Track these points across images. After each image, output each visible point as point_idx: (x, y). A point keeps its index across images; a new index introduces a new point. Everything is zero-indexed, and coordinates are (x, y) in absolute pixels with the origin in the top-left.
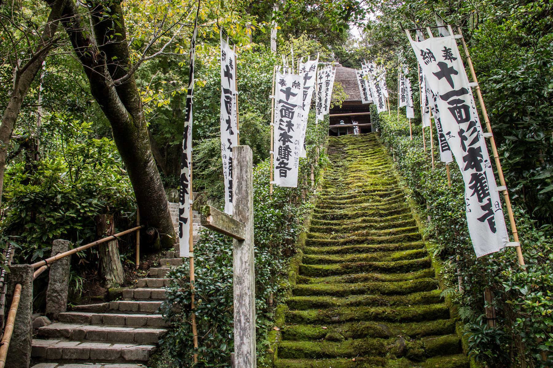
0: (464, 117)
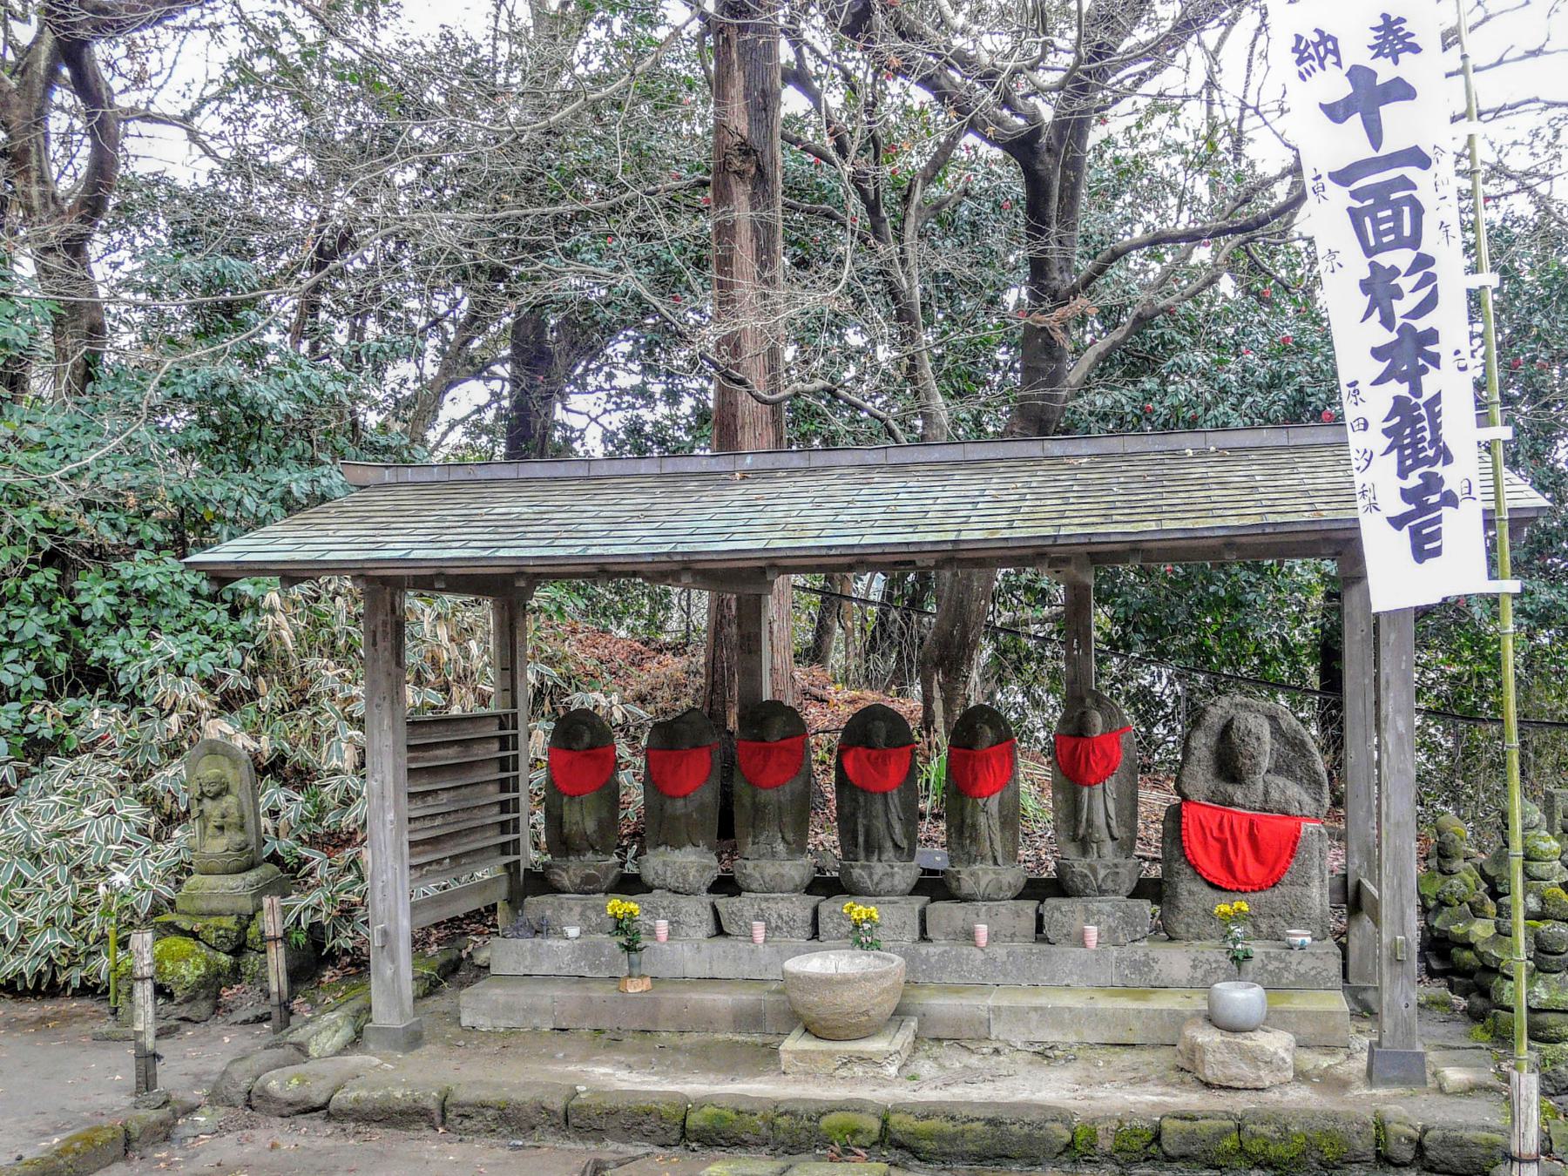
0: (1407, 232)
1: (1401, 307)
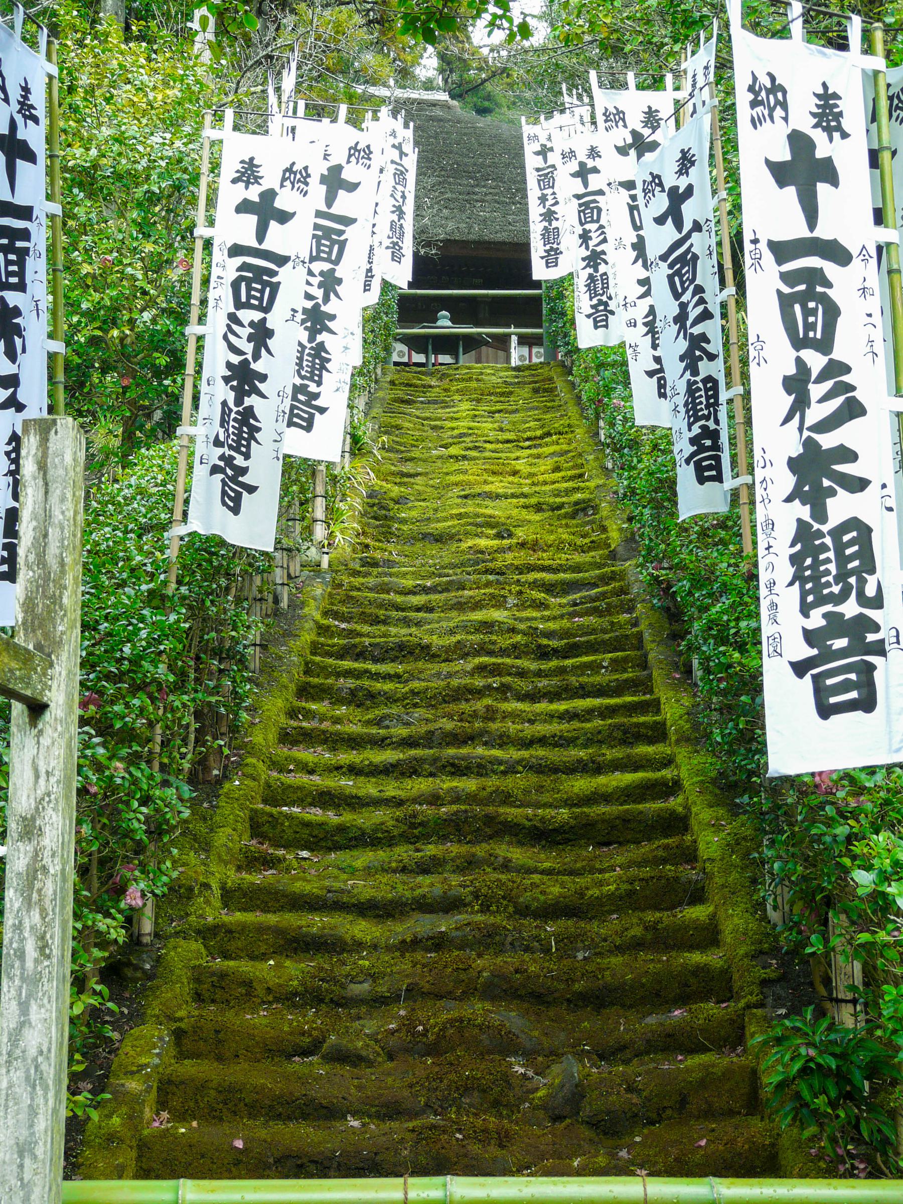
1: (591, 243)
